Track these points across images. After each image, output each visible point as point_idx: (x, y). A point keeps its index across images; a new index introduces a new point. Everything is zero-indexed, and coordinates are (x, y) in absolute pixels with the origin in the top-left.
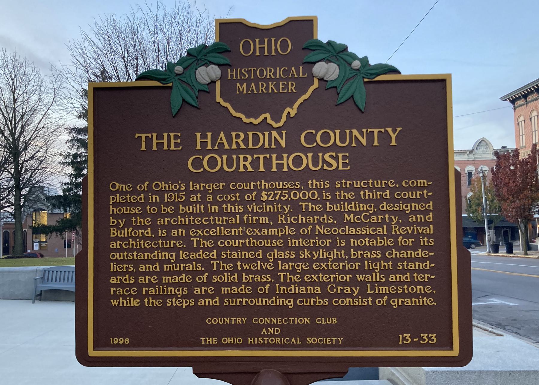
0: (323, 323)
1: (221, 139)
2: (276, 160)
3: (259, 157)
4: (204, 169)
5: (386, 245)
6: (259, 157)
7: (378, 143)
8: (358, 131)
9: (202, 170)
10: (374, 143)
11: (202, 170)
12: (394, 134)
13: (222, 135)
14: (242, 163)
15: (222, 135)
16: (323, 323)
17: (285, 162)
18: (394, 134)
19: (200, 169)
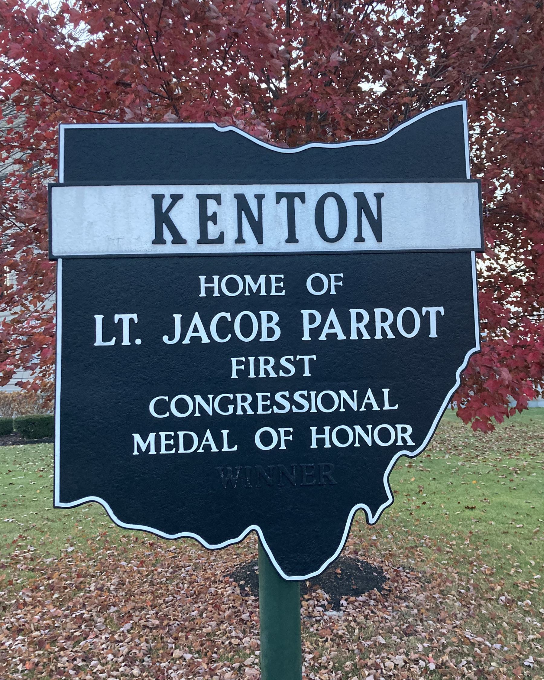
0: (181, 450)
1: (369, 399)
2: (317, 434)
3: (303, 359)
4: (171, 413)
5: (314, 410)
6: (303, 359)
7: (94, 320)
8: (203, 398)
9: (167, 415)
10: (95, 341)
11: (167, 415)
12: (193, 332)
13: (370, 393)
14: (262, 366)
15: (370, 393)
16: (181, 450)
17: (327, 436)
18: (193, 332)
19: (166, 413)
